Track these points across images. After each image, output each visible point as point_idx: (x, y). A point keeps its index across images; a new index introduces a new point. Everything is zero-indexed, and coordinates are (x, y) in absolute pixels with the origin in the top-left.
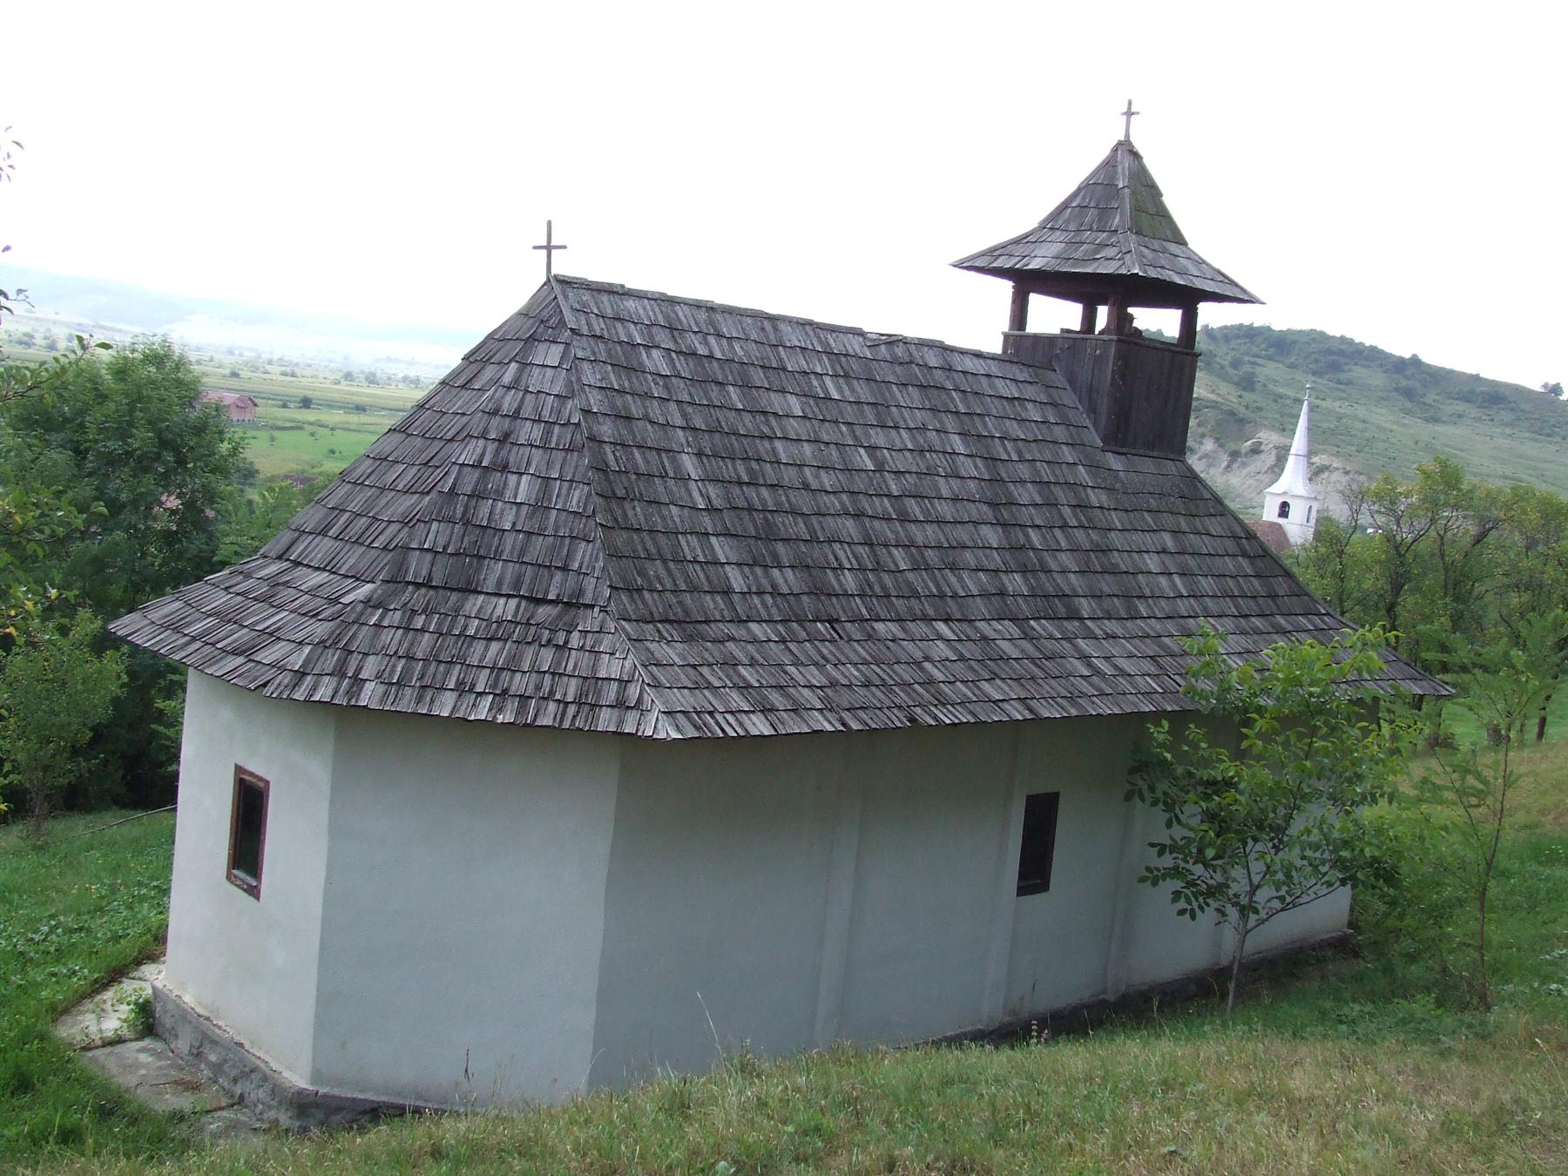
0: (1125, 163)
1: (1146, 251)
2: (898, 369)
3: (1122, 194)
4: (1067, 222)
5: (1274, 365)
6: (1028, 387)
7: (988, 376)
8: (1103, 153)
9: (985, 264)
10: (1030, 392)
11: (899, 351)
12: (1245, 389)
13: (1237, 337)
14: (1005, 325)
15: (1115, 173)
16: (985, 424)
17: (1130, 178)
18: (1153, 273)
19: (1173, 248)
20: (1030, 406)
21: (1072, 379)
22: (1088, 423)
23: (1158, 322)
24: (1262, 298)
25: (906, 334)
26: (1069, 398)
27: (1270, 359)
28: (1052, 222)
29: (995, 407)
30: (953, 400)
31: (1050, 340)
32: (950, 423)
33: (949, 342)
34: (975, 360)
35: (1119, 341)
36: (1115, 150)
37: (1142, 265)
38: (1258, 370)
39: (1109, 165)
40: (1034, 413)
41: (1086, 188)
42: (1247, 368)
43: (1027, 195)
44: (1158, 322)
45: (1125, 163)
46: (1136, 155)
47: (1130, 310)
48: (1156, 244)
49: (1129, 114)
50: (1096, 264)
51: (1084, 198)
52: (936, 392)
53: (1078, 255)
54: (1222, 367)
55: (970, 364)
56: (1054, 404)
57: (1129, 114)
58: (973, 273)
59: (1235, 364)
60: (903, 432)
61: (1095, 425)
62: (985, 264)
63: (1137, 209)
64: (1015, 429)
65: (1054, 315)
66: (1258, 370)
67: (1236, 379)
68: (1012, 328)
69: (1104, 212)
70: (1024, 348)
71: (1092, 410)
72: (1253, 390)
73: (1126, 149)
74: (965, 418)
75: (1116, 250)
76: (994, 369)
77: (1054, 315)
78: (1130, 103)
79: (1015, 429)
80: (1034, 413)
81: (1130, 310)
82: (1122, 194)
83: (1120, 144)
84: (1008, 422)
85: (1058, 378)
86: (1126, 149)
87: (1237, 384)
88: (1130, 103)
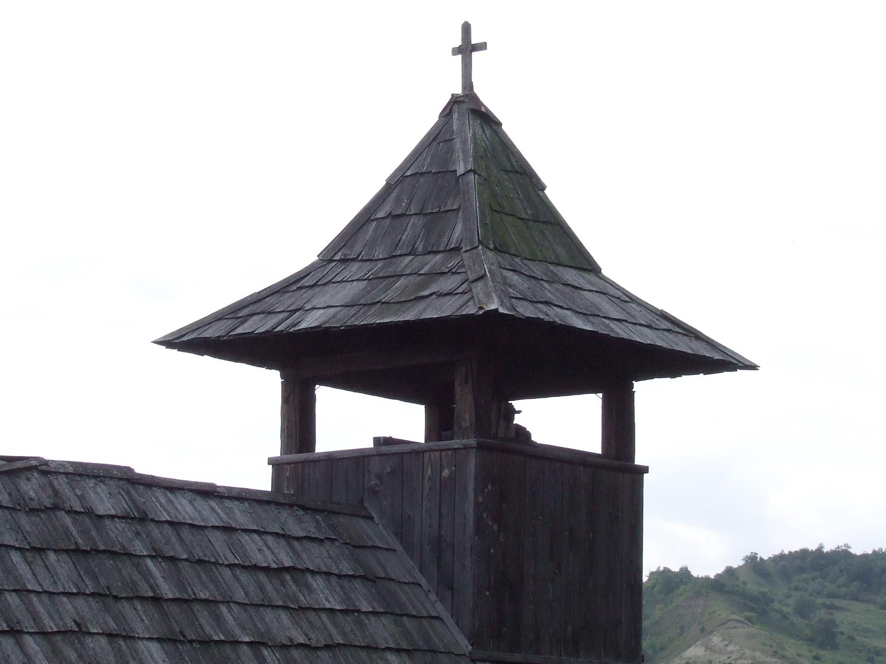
0: (467, 131)
1: (514, 278)
2: (24, 520)
3: (468, 180)
4: (372, 244)
5: (863, 606)
6: (315, 548)
7: (227, 529)
8: (429, 119)
9: (222, 338)
10: (317, 557)
11: (31, 487)
12: (822, 646)
13: (802, 570)
14: (272, 445)
15: (450, 151)
16: (218, 620)
17: (477, 157)
18: (526, 311)
19: (571, 276)
20: (318, 583)
21: (402, 529)
22: (440, 609)
23: (562, 421)
24: (754, 360)
25: (48, 456)
26: (399, 566)
27: (855, 598)
28: (342, 251)
29: (243, 587)
30: (147, 576)
31: (354, 461)
32: (139, 620)
33: (142, 468)
34: (200, 502)
35: (480, 447)
36: (447, 113)
37: (504, 290)
38: (839, 616)
39: (438, 139)
40: (324, 594)
41: (398, 182)
42: (822, 614)
43: (291, 213)
44: (562, 421)
45: (467, 131)
46: (488, 120)
47: (517, 404)
48: (536, 269)
49: (467, 49)
50: (421, 306)
51: (398, 200)
52: (109, 562)
53: (390, 295)
54: (785, 617)
55: (186, 509)
56: (369, 579)
57: (467, 49)
58: (207, 361)
59: (803, 610)
60: (30, 642)
61: (455, 614)
62: (222, 338)
63: (495, 209)
64: (284, 627)
65: (355, 420)
66: (839, 616)
67: (807, 632)
68: (286, 447)
69: (436, 220)
70: (306, 473)
71: (446, 585)
72: (835, 647)
73: (467, 111)
74: (174, 609)
75: (457, 279)
76: (241, 517)
77: (355, 420)
78: (466, 29)
79: (284, 627)
80: (324, 594)
81: (517, 404)
82: (468, 180)
83: (455, 101)
84: (269, 615)
85: (376, 532)
86: (467, 111)
87: (811, 640)
88: (466, 29)
